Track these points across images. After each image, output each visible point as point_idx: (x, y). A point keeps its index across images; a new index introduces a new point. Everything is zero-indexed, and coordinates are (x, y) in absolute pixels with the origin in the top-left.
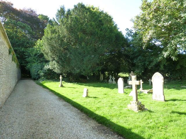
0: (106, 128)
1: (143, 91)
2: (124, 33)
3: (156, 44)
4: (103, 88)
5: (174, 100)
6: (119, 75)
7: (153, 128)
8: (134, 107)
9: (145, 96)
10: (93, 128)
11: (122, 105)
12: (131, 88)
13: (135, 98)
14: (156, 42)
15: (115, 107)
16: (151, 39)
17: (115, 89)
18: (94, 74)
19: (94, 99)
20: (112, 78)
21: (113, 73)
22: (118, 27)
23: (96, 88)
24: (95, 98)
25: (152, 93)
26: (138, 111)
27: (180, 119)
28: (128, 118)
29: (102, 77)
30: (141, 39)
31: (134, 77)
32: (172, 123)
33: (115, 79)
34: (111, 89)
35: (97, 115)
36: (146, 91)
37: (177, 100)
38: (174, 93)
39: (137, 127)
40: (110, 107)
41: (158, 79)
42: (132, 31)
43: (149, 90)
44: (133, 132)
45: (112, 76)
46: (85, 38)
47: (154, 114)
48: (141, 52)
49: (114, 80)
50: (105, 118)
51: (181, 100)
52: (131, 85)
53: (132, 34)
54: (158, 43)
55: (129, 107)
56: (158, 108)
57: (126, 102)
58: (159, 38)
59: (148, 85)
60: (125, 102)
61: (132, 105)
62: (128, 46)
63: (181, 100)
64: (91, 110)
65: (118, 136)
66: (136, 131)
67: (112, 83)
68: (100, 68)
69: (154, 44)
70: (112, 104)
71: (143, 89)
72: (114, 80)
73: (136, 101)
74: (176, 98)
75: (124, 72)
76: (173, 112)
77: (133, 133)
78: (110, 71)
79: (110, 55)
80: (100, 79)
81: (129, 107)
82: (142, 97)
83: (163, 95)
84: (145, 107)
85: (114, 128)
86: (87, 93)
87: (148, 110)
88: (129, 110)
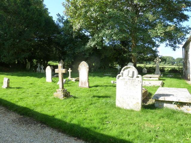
0: (28, 118)
1: (71, 79)
2: (55, 19)
3: (86, 34)
4: (30, 77)
5: (97, 86)
6: (48, 63)
7: (75, 112)
8: (59, 94)
9: (73, 84)
10: (13, 121)
11: (48, 94)
12: (58, 76)
13: (61, 86)
14: (85, 32)
15: (41, 97)
16: (81, 29)
17: (43, 79)
18: (18, 61)
19: (18, 89)
20: (41, 66)
21: (42, 61)
22: (49, 11)
23: (20, 77)
24: (19, 88)
25: (78, 81)
26: (64, 98)
27: (99, 102)
28: (53, 105)
29: (28, 66)
30: (71, 27)
31: (60, 65)
32: (92, 106)
33: (71, 71)
34: (38, 78)
35: (19, 106)
36: (74, 80)
37: (99, 86)
38: (98, 80)
39: (60, 113)
40: (36, 97)
41: (83, 68)
42: (64, 18)
43: (76, 78)
44: (121, 138)
45: (41, 64)
46: (7, 17)
47: (78, 99)
48: (71, 40)
49: (42, 69)
50: (28, 108)
51: (102, 86)
52: (58, 74)
53: (63, 21)
54: (87, 34)
55: (55, 94)
56: (83, 94)
57: (53, 89)
58: (89, 28)
59: (76, 74)
60: (52, 90)
61: (58, 93)
62: (59, 33)
63: (102, 86)
64: (12, 101)
65: (42, 124)
66: (59, 117)
67: (40, 72)
68: (27, 55)
69: (84, 34)
70: (38, 94)
71: (71, 78)
72: (42, 69)
73: (62, 89)
74: (99, 84)
75: (54, 61)
76: (94, 97)
77: (56, 119)
78: (39, 59)
79: (39, 41)
80: (27, 67)
81: (55, 94)
82: (69, 85)
83: (88, 82)
84: (71, 94)
85: (38, 117)
86: (8, 83)
87: (73, 96)
88: (55, 98)
